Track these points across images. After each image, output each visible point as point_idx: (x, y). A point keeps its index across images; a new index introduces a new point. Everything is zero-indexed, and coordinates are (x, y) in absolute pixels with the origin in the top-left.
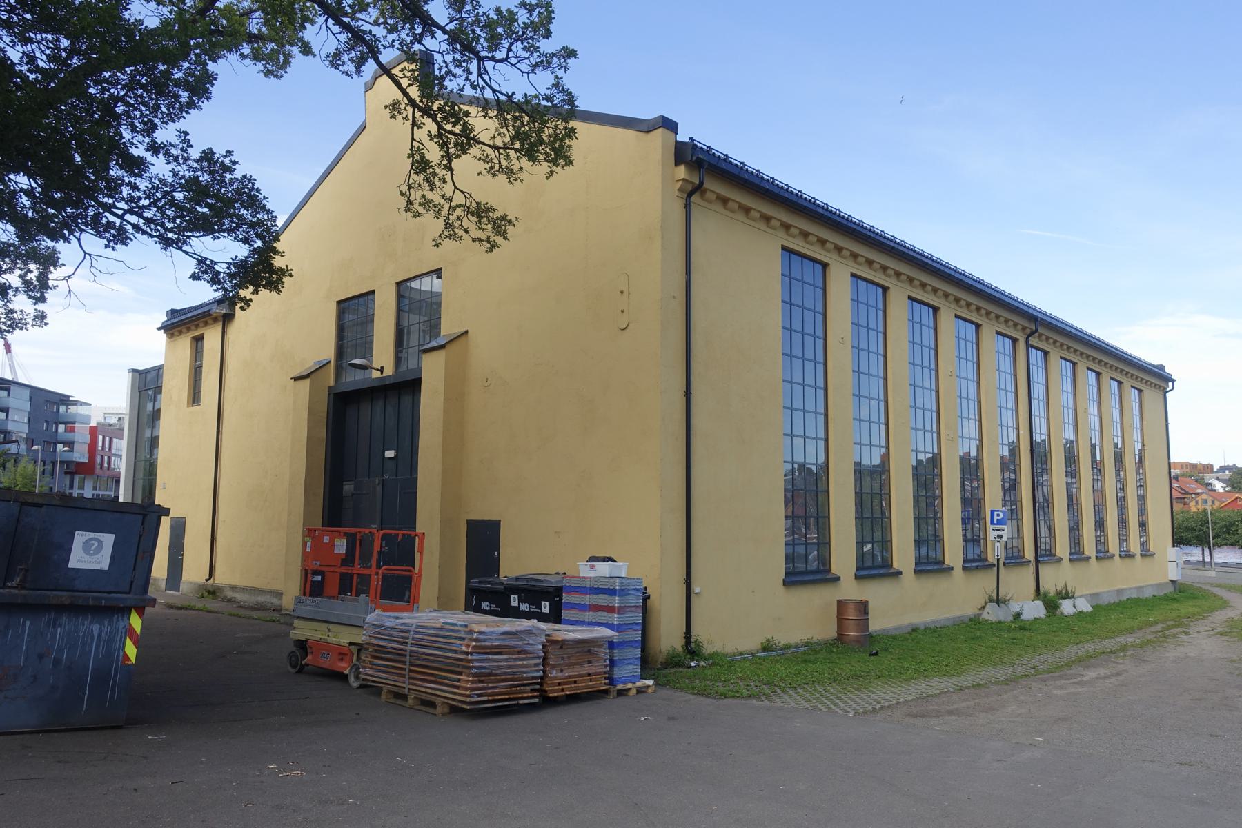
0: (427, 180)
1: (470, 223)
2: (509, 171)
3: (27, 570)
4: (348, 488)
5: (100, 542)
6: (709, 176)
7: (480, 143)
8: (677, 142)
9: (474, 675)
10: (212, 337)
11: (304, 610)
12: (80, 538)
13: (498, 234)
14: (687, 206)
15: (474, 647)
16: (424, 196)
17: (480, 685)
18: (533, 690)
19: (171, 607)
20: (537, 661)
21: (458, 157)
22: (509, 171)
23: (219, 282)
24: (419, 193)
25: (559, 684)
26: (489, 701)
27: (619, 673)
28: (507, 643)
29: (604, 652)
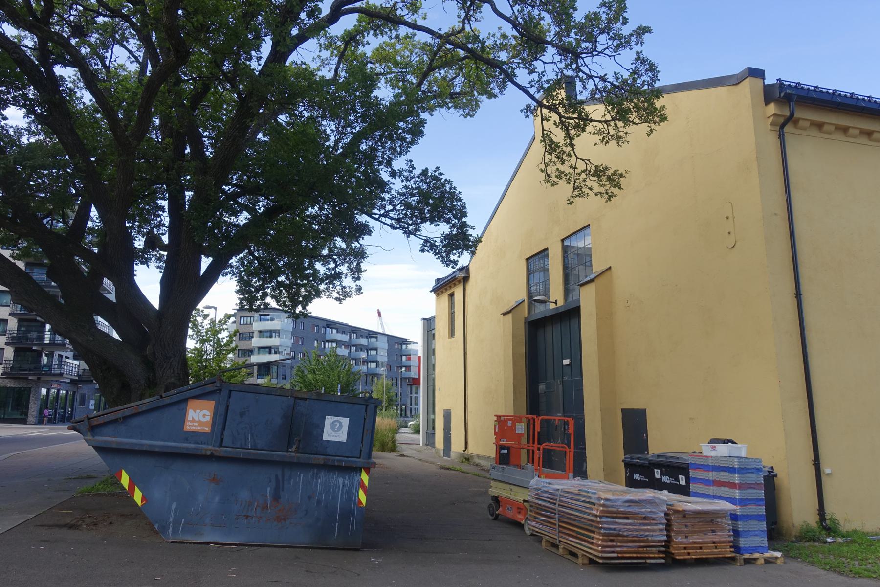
0: (558, 157)
1: (592, 182)
2: (618, 138)
3: (299, 441)
4: (542, 387)
5: (340, 423)
6: (795, 105)
7: (594, 121)
8: (765, 86)
9: (604, 535)
10: (458, 292)
11: (495, 474)
12: (329, 420)
13: (615, 186)
14: (781, 137)
15: (602, 511)
16: (558, 170)
17: (610, 544)
18: (660, 552)
19: (442, 468)
20: (661, 527)
21: (579, 136)
22: (618, 138)
23: (439, 253)
24: (554, 168)
25: (685, 548)
26: (618, 558)
27: (743, 542)
28: (631, 510)
29: (727, 522)
